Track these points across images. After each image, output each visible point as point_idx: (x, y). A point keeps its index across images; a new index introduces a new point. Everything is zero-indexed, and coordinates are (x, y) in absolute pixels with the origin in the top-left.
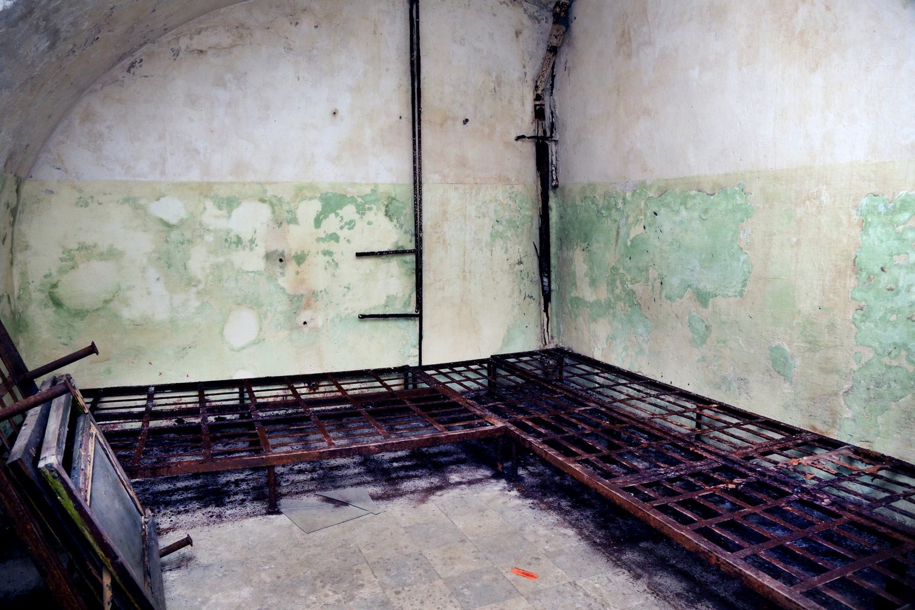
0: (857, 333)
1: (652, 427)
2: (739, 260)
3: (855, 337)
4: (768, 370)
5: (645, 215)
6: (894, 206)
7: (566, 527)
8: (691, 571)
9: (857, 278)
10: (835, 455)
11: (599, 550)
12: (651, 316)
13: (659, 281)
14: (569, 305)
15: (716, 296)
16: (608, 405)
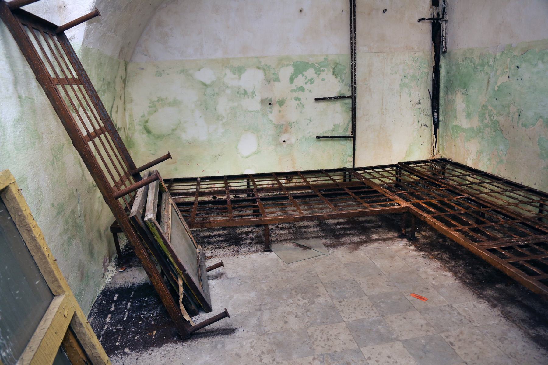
1: (508, 211)
5: (510, 68)
7: (446, 271)
11: (468, 287)
13: (517, 114)
16: (476, 196)
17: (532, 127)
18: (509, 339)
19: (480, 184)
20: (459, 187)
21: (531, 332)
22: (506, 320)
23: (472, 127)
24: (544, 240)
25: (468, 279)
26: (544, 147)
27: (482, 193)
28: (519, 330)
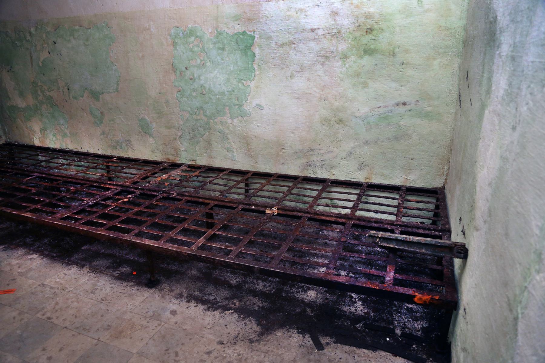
0: (179, 105)
1: (77, 179)
2: (112, 69)
3: (179, 107)
4: (140, 133)
5: (48, 44)
6: (187, 33)
7: (32, 254)
8: (113, 253)
9: (175, 74)
10: (179, 171)
11: (56, 260)
12: (66, 111)
13: (66, 88)
14: (8, 112)
15: (103, 93)
16: (47, 172)
17: (82, 99)
18: (99, 288)
19: (50, 161)
20: (27, 168)
21: (116, 273)
22: (95, 273)
23: (28, 105)
24: (108, 195)
25: (55, 253)
26: (96, 116)
27: (51, 168)
28: (106, 277)
